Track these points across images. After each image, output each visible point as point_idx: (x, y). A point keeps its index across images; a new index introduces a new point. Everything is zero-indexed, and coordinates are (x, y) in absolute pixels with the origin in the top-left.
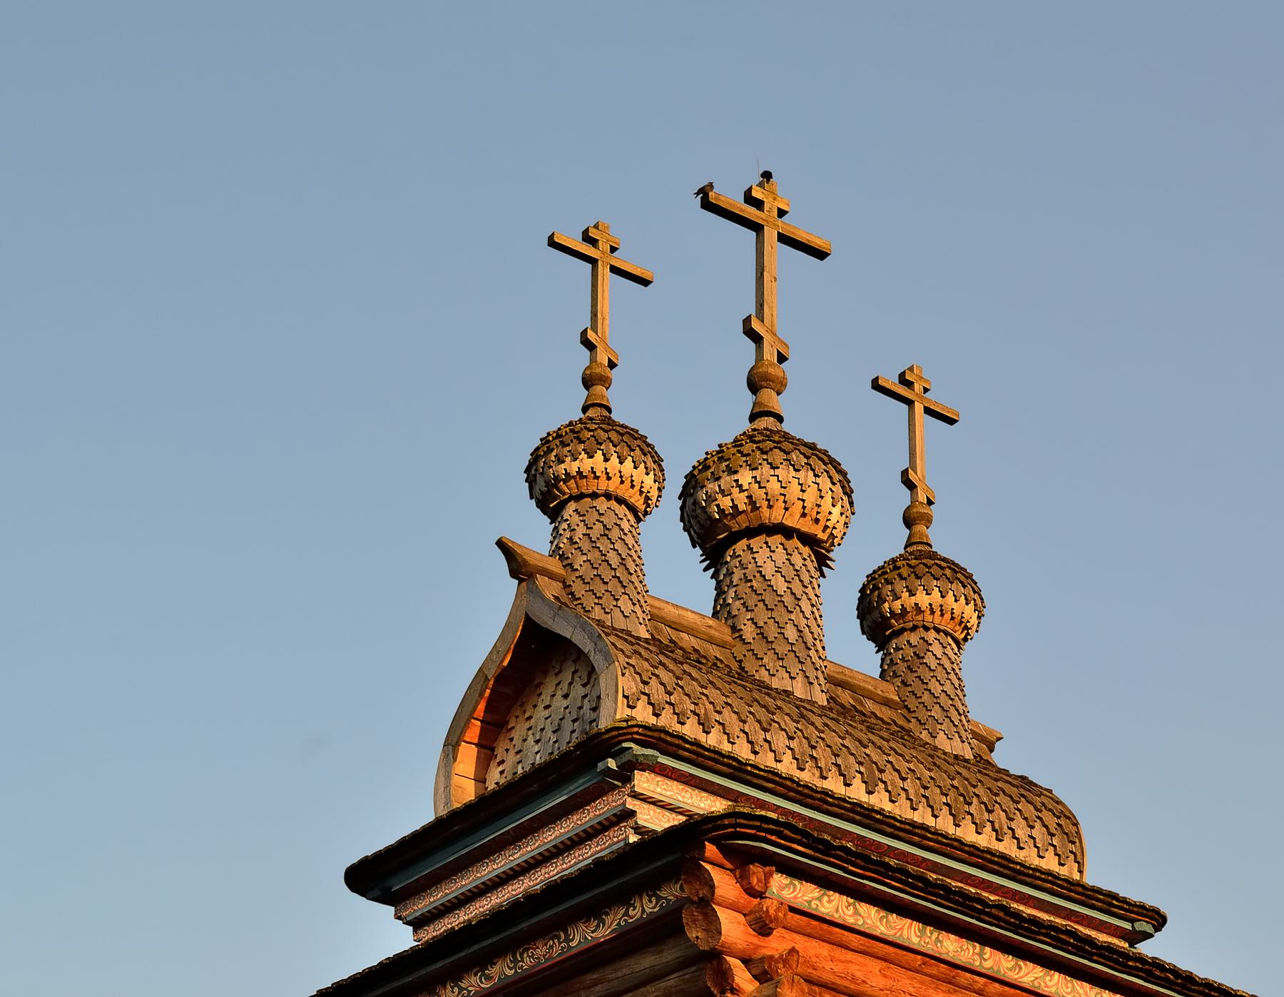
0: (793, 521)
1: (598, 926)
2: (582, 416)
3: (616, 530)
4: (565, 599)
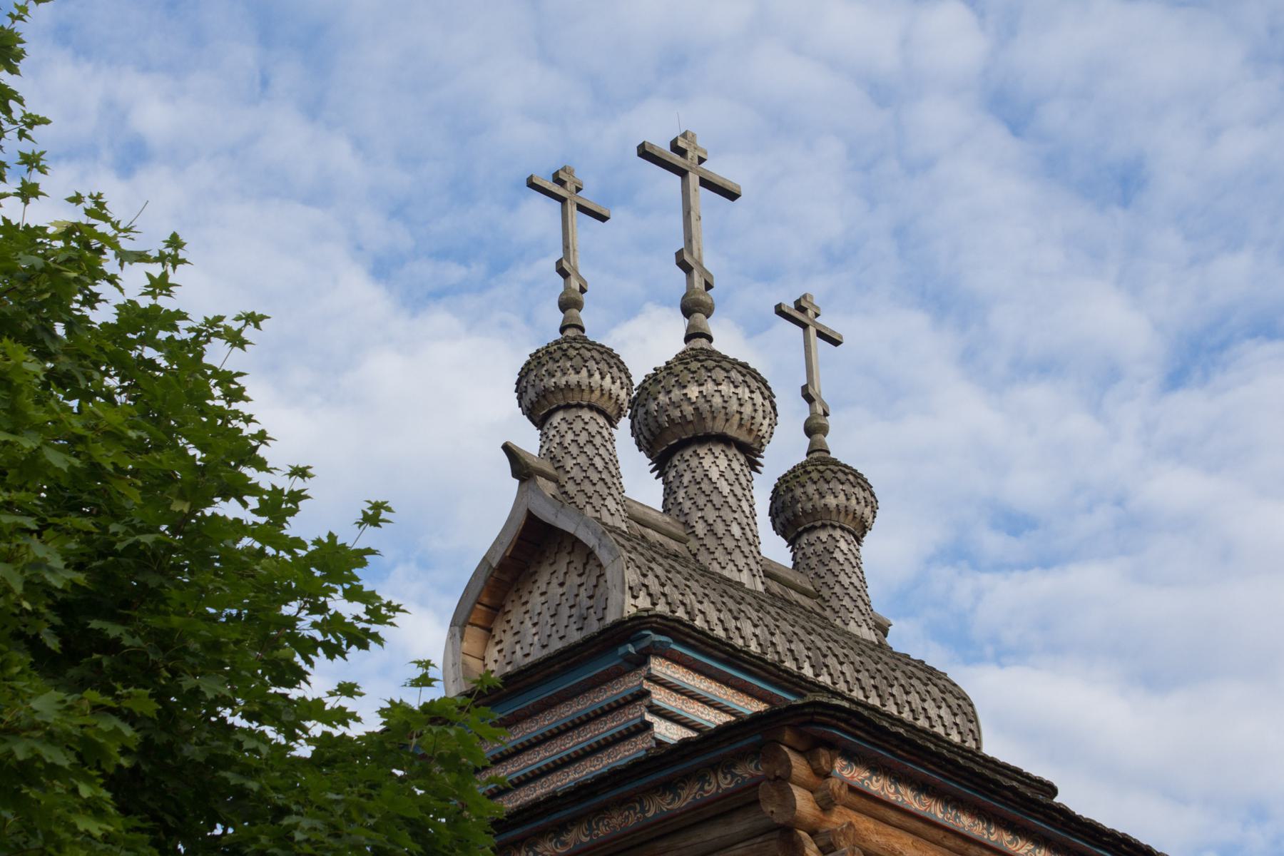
0: (732, 431)
1: (673, 799)
2: (559, 336)
3: (598, 437)
4: (560, 497)
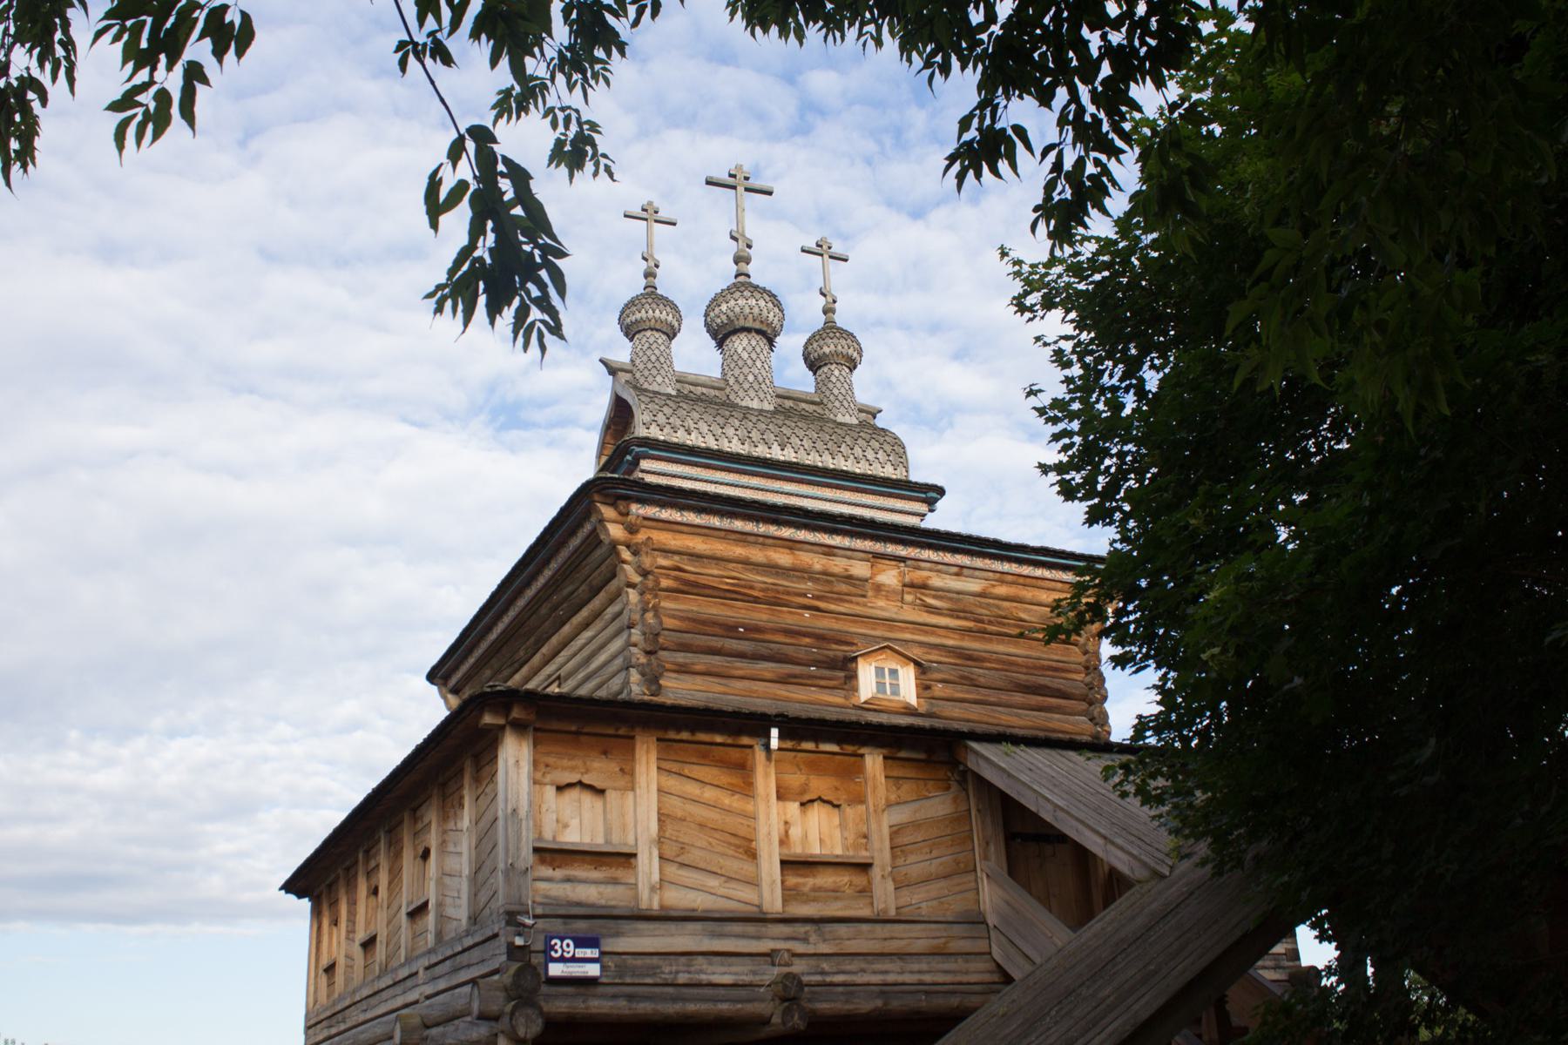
0: (749, 324)
